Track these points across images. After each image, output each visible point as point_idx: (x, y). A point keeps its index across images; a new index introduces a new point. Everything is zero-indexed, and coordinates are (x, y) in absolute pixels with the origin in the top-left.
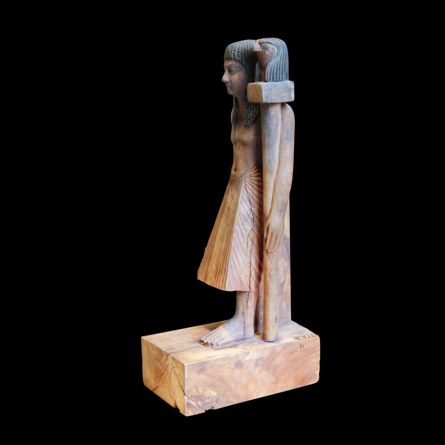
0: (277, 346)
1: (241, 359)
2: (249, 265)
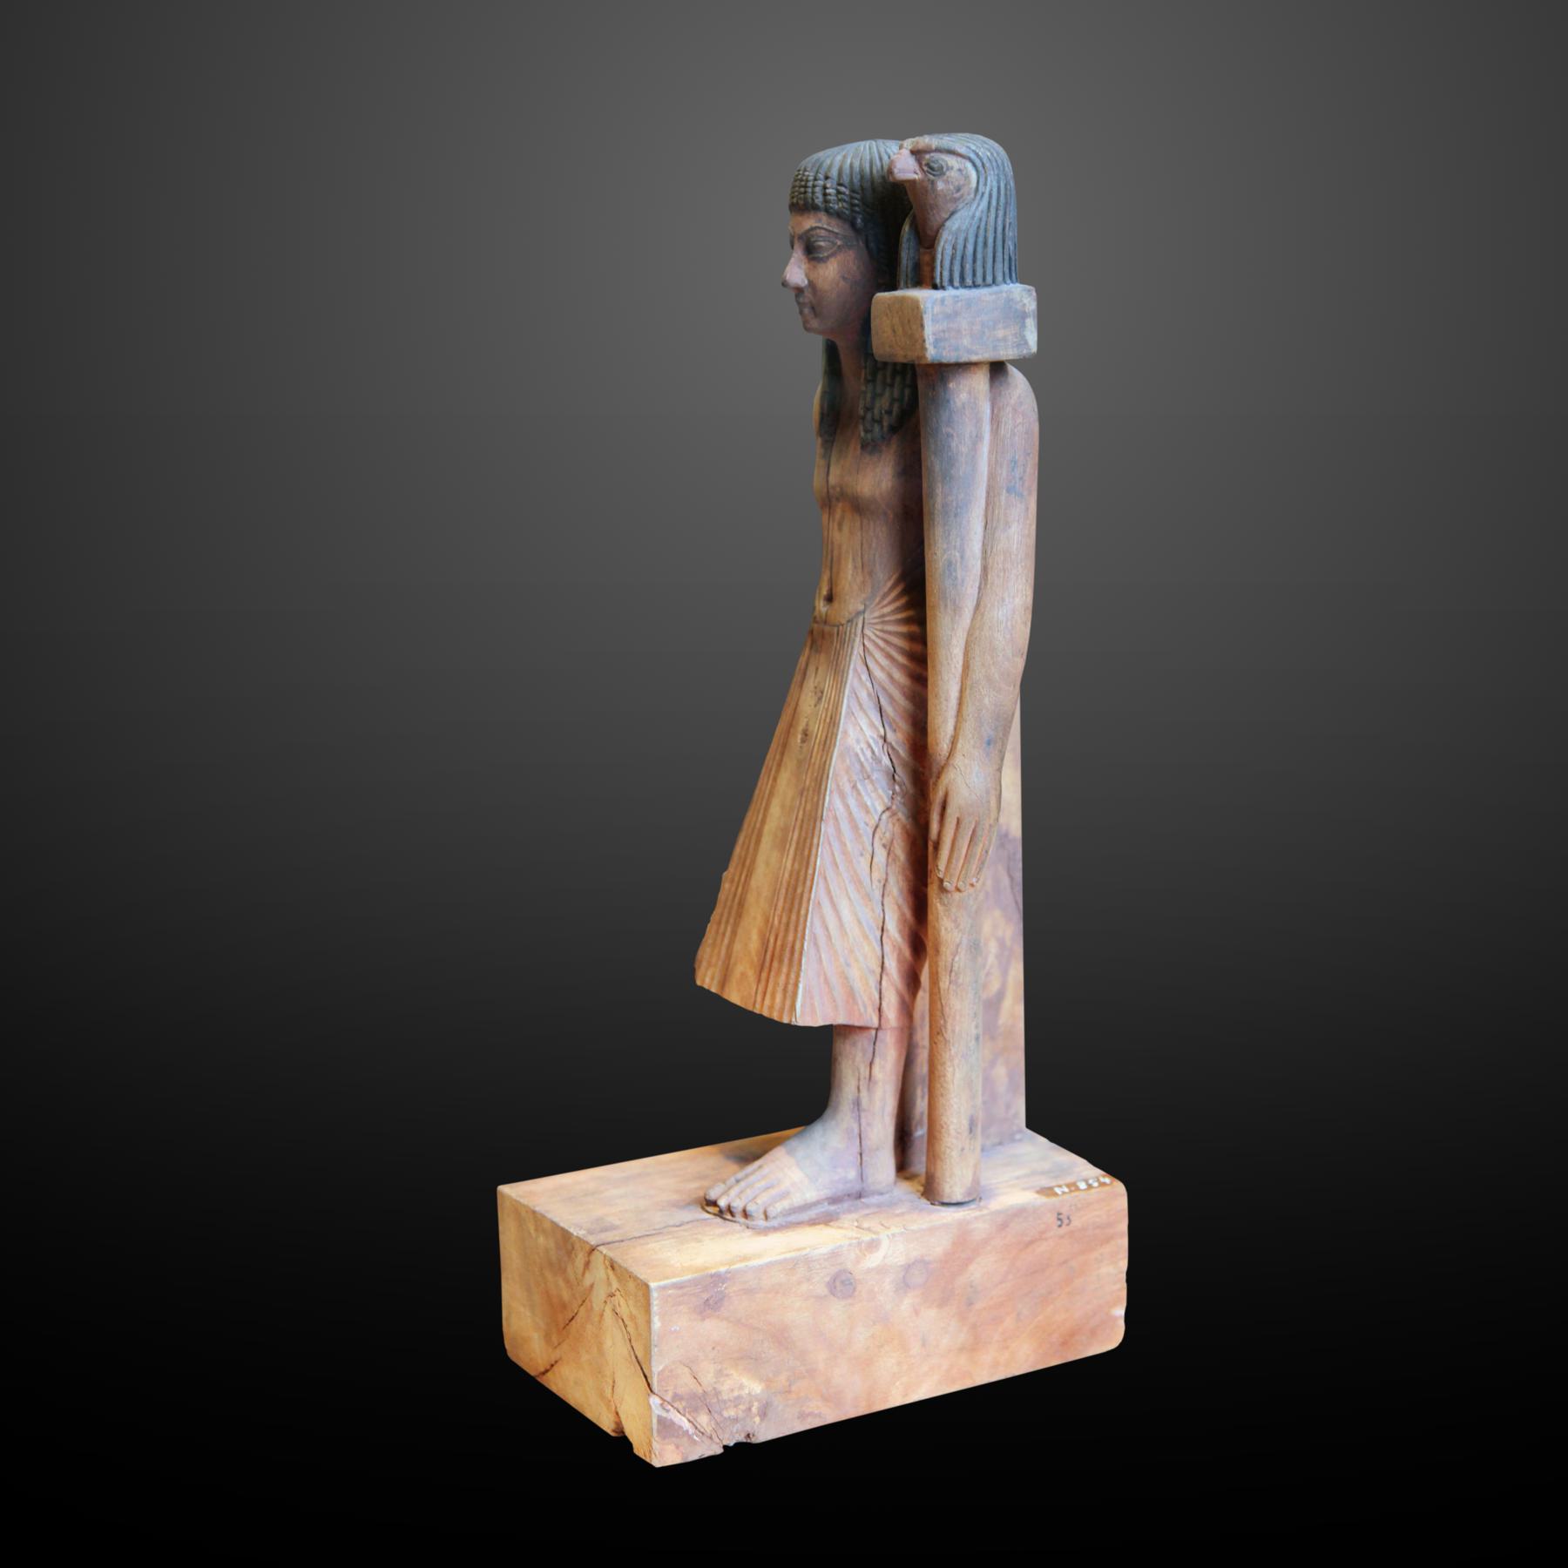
0: (976, 1218)
1: (849, 1266)
2: (878, 934)
